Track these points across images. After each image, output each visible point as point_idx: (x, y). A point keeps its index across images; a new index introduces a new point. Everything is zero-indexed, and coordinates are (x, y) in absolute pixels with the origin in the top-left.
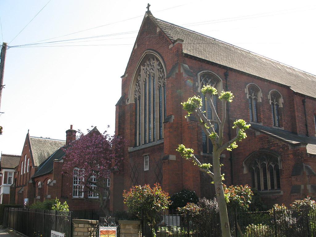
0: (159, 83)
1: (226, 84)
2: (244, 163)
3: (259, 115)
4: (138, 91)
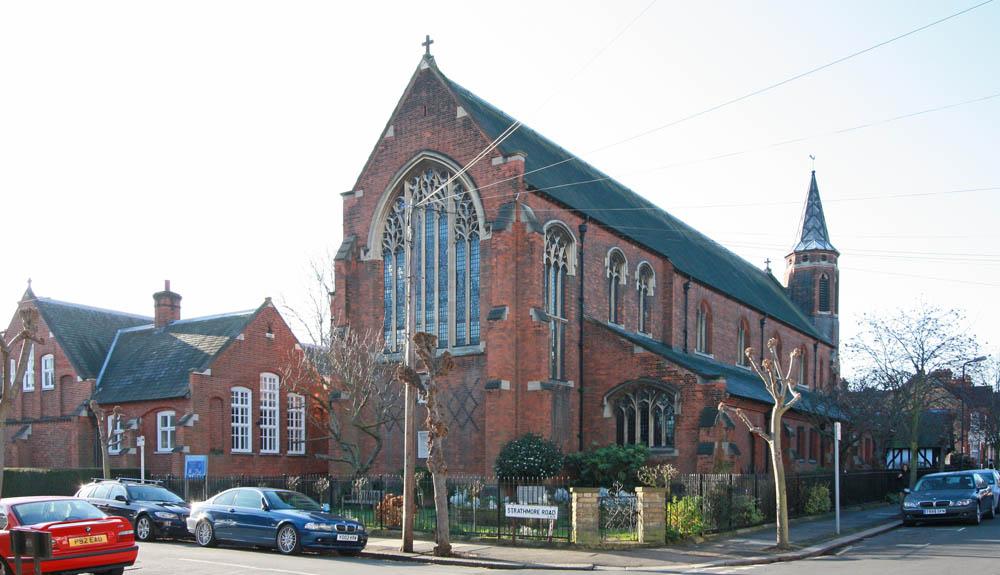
0: (459, 232)
1: (582, 247)
2: (605, 399)
3: (619, 309)
4: (395, 237)
